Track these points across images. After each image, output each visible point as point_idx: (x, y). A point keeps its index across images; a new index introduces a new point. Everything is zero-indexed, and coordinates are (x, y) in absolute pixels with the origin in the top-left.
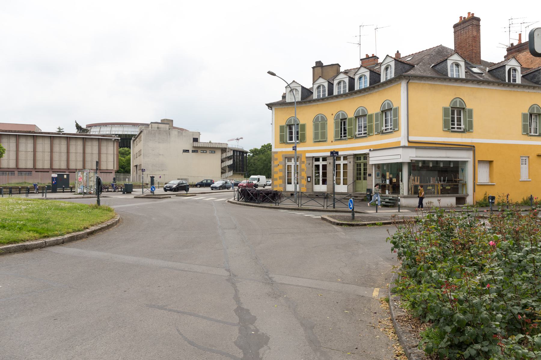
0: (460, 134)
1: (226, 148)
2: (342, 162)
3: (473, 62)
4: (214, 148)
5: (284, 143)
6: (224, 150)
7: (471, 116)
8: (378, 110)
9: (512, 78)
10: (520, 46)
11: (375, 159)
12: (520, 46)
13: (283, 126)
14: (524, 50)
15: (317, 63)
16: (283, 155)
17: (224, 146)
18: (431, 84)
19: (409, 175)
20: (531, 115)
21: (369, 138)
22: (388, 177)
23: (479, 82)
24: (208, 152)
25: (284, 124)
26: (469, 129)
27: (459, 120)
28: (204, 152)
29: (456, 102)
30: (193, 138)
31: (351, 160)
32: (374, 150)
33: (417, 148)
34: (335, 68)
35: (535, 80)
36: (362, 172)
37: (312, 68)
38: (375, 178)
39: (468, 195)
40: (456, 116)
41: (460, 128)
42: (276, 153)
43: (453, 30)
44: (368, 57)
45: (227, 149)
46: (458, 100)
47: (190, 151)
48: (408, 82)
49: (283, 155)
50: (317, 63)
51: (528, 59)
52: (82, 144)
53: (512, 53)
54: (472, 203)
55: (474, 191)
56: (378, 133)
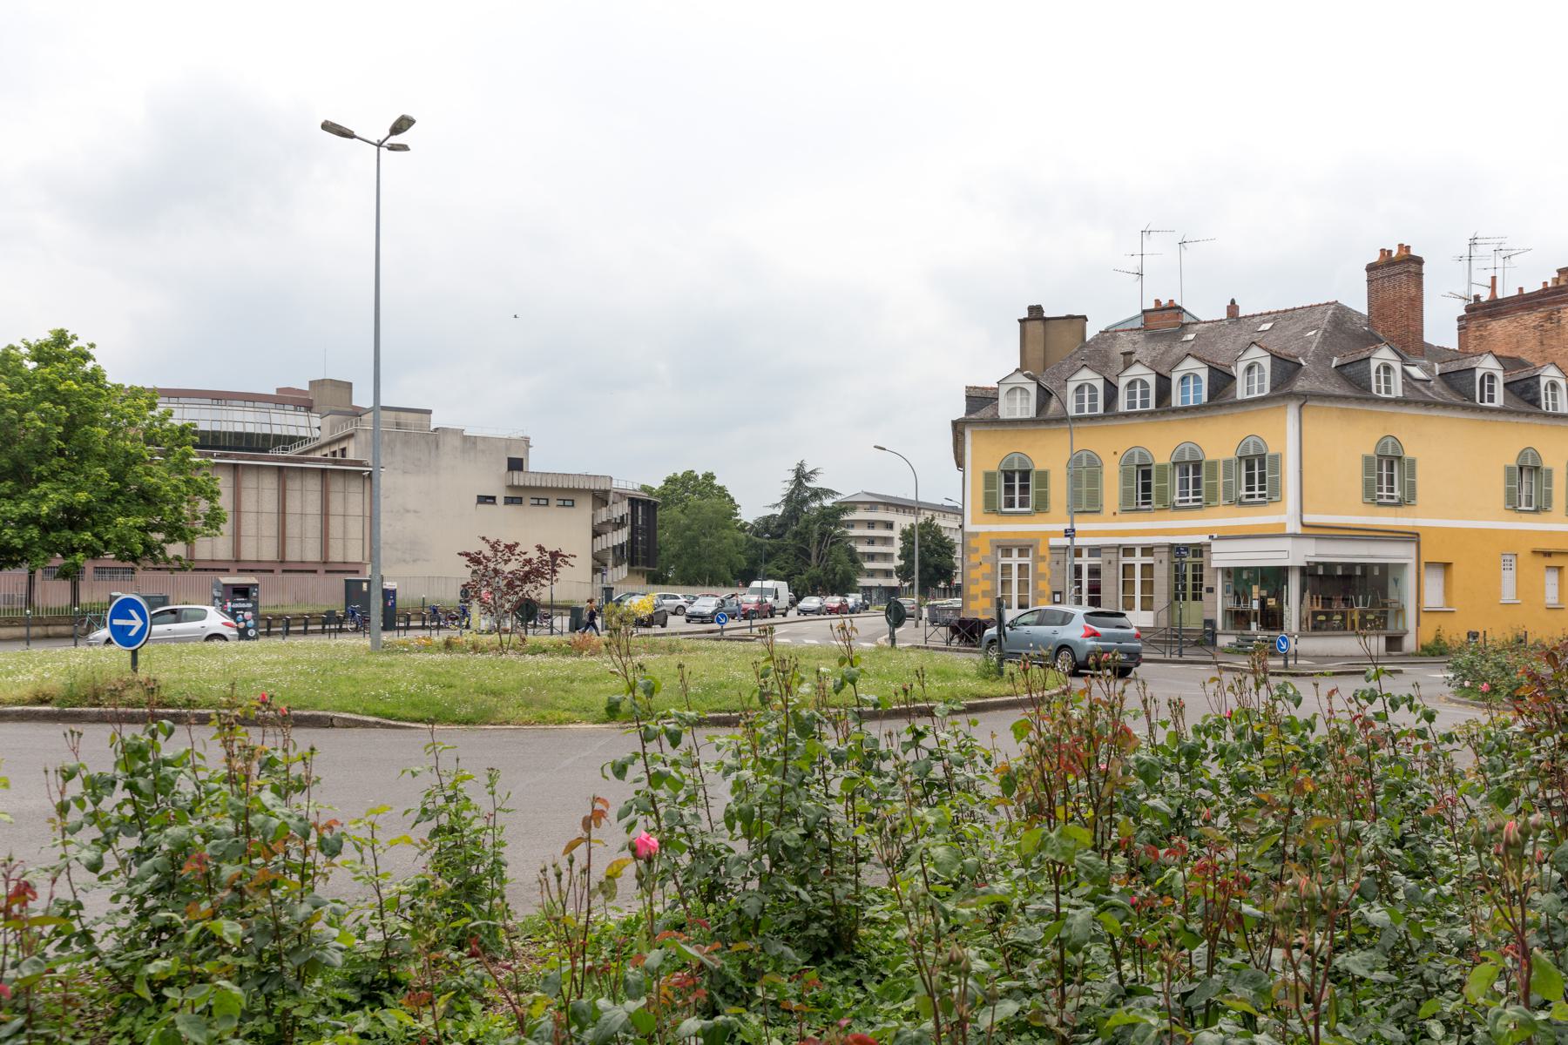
0: (1393, 509)
1: (607, 492)
2: (1138, 560)
3: (1408, 353)
4: (546, 489)
5: (995, 511)
6: (601, 498)
7: (1412, 474)
8: (1230, 453)
9: (1486, 393)
10: (1495, 306)
11: (1224, 556)
12: (1495, 306)
13: (994, 474)
14: (1502, 314)
15: (1031, 309)
16: (991, 542)
17: (602, 486)
18: (1342, 409)
19: (1303, 590)
20: (1521, 469)
21: (1208, 511)
22: (1255, 596)
23: (1428, 404)
24: (553, 502)
25: (994, 467)
26: (1407, 500)
27: (1391, 480)
28: (542, 502)
29: (1386, 444)
30: (509, 459)
31: (1165, 556)
32: (1220, 538)
33: (1318, 538)
34: (1076, 324)
35: (1529, 396)
36: (1189, 582)
37: (1020, 321)
38: (1223, 597)
39: (1406, 632)
40: (1385, 473)
41: (1392, 497)
42: (976, 534)
43: (1365, 275)
44: (1159, 309)
45: (611, 495)
46: (1390, 440)
47: (500, 500)
48: (1301, 406)
49: (991, 542)
50: (1031, 309)
51: (1510, 336)
52: (275, 485)
53: (1476, 318)
54: (1413, 649)
55: (1418, 624)
56: (1231, 503)
